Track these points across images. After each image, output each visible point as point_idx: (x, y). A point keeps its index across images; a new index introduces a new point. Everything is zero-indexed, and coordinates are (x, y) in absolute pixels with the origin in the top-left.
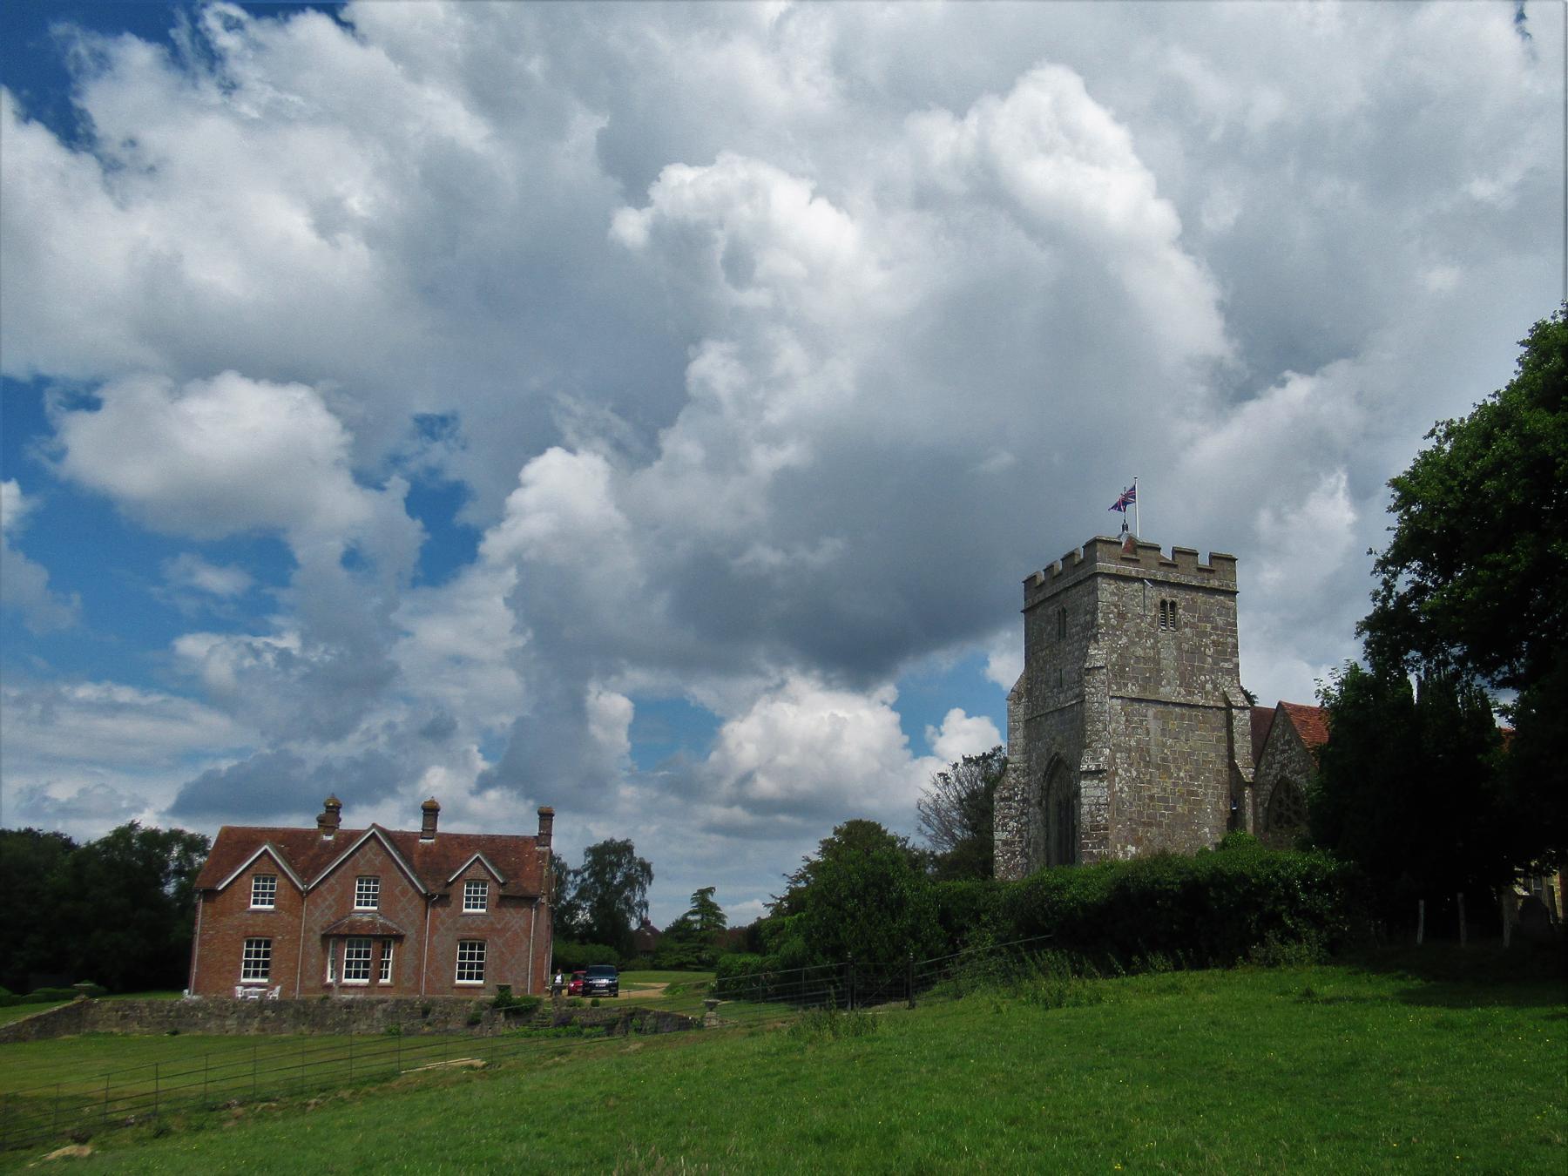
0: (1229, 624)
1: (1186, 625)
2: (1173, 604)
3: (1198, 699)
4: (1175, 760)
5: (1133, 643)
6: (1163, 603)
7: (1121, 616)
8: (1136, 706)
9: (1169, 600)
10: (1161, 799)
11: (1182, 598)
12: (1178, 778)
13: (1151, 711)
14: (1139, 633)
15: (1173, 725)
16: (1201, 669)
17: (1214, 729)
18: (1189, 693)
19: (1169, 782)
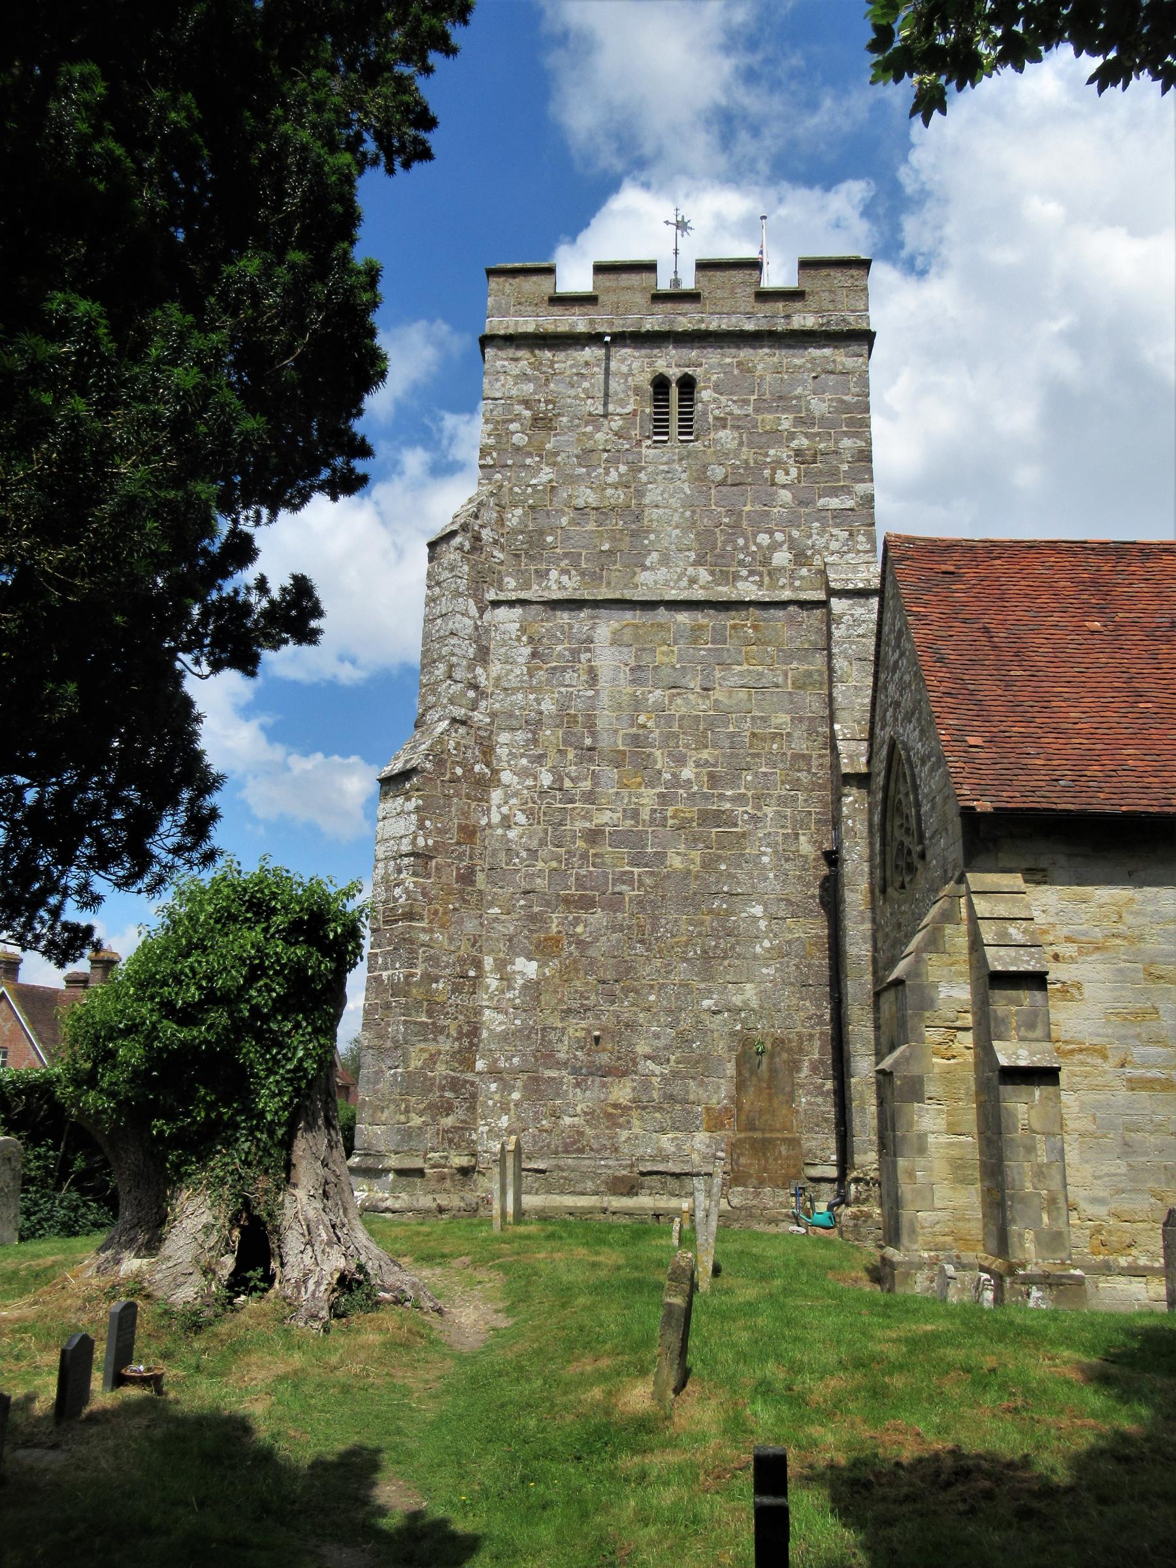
0: (845, 407)
1: (722, 423)
2: (688, 385)
3: (748, 590)
4: (668, 737)
5: (572, 480)
6: (660, 385)
7: (542, 423)
8: (564, 617)
9: (674, 373)
10: (620, 838)
11: (708, 365)
12: (676, 782)
13: (606, 627)
14: (586, 455)
15: (665, 656)
16: (760, 521)
17: (789, 657)
18: (773, 587)
19: (648, 798)
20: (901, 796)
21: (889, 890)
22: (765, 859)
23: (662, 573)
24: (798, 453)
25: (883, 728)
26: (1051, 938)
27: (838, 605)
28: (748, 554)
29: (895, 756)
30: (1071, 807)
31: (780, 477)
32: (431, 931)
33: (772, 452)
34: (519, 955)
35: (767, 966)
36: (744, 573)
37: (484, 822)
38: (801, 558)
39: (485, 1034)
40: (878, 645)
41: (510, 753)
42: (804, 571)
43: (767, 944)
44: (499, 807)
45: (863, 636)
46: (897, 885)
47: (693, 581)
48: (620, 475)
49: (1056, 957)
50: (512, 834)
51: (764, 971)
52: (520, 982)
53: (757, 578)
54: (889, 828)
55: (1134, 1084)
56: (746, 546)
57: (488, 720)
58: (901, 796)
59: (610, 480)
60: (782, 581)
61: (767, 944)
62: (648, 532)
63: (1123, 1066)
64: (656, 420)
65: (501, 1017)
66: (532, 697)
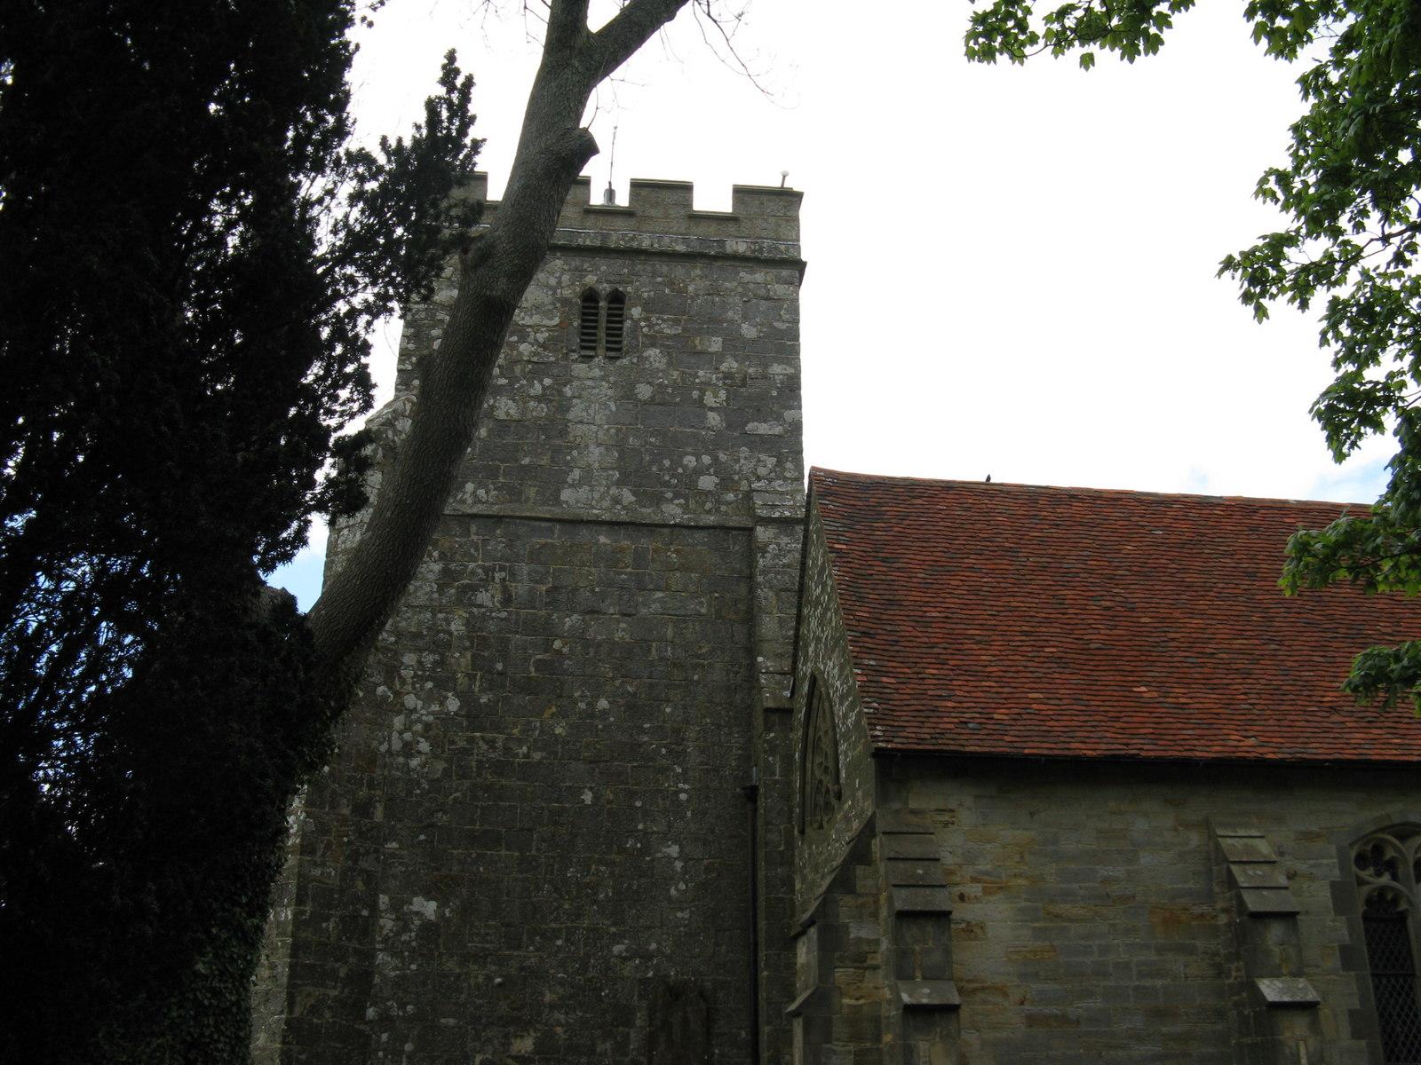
2: (617, 298)
6: (590, 297)
9: (605, 288)
12: (591, 714)
20: (821, 733)
21: (808, 830)
22: (683, 796)
23: (583, 492)
24: (728, 376)
25: (805, 664)
26: (958, 879)
27: (762, 534)
28: (673, 476)
29: (816, 692)
30: (978, 749)
31: (709, 400)
32: (323, 864)
33: (701, 373)
34: (416, 894)
35: (682, 910)
36: (669, 495)
37: (383, 748)
38: (726, 482)
39: (377, 979)
40: (802, 577)
41: (416, 675)
42: (731, 496)
43: (682, 886)
44: (401, 733)
45: (789, 566)
46: (816, 825)
47: (616, 500)
48: (544, 388)
49: (962, 897)
50: (414, 763)
51: (679, 915)
52: (417, 922)
53: (682, 501)
54: (809, 765)
55: (1031, 1020)
56: (672, 469)
57: (393, 639)
58: (821, 733)
59: (532, 392)
60: (708, 506)
61: (682, 886)
62: (571, 448)
63: (1022, 1003)
64: (594, 341)
65: (397, 962)
66: (440, 616)
